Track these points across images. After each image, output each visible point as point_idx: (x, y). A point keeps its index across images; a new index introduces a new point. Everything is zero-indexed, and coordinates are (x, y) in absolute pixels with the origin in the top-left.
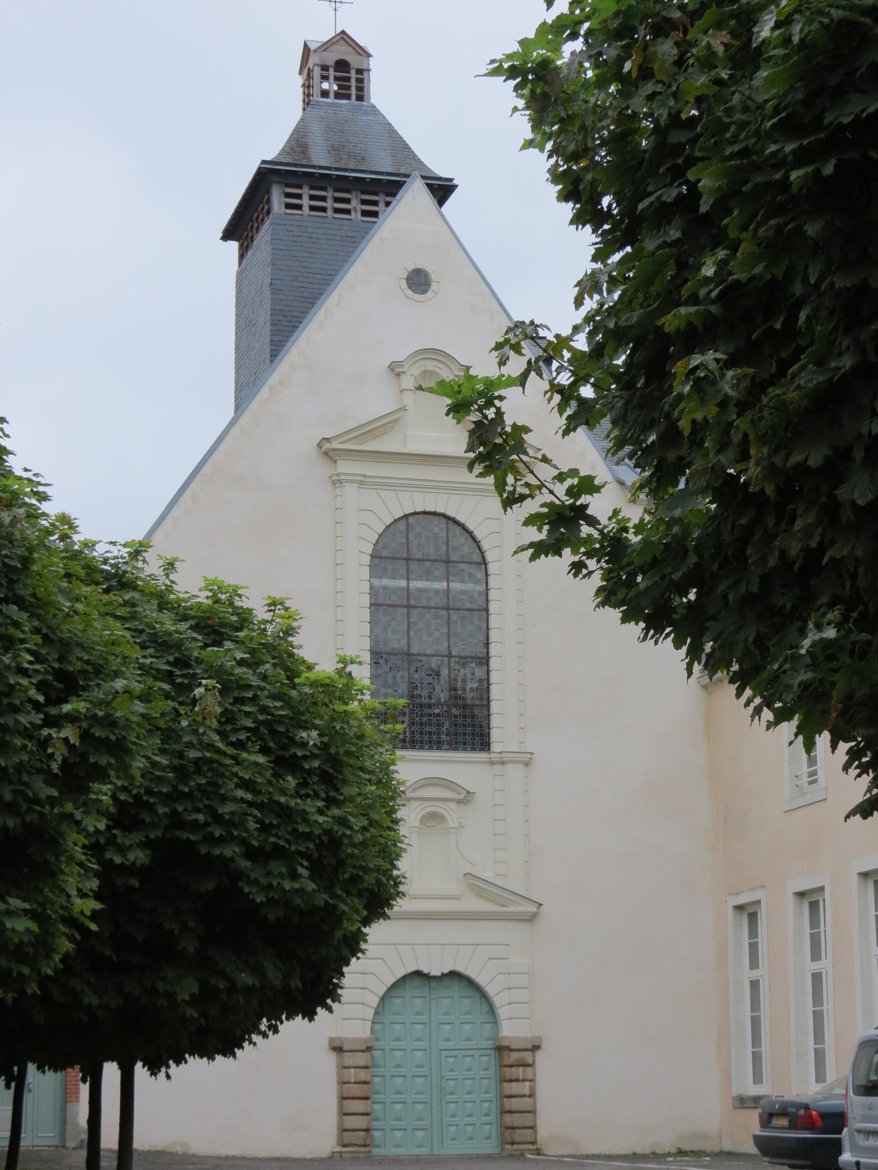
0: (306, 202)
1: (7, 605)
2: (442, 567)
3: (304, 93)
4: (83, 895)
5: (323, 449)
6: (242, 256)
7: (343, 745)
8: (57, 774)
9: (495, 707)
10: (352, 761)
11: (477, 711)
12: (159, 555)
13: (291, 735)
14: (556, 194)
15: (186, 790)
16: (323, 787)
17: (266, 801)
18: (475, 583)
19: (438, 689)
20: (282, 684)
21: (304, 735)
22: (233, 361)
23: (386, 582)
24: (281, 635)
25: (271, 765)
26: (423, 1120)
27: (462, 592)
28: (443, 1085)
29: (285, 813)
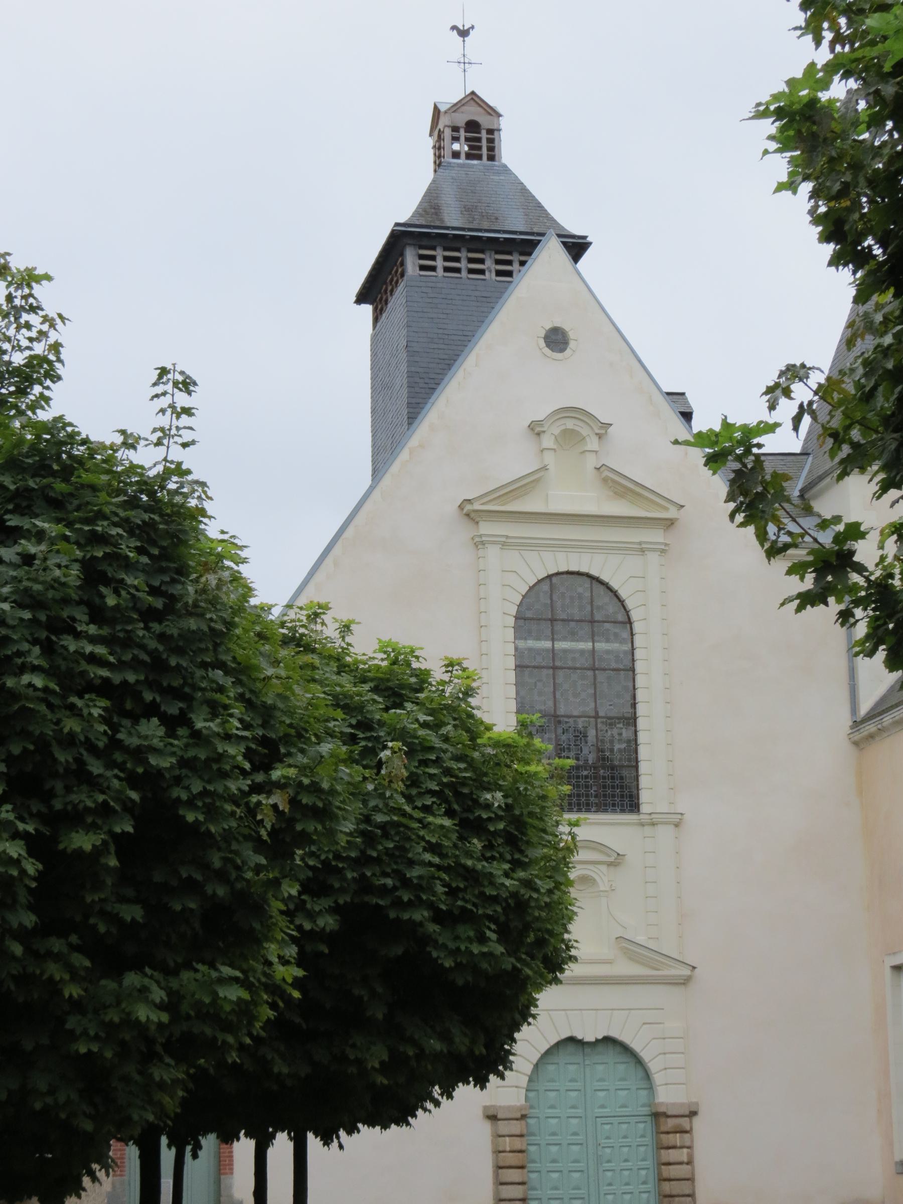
0: (440, 263)
1: (213, 670)
2: (587, 627)
3: (435, 154)
4: (284, 962)
5: (465, 511)
6: (376, 320)
7: (527, 806)
8: (266, 841)
9: (643, 767)
10: (536, 822)
11: (625, 773)
12: (334, 618)
13: (475, 797)
14: (817, 236)
15: (375, 854)
16: (508, 849)
17: (453, 864)
18: (621, 643)
19: (585, 751)
20: (464, 745)
21: (488, 796)
22: (369, 424)
23: (531, 643)
24: (461, 695)
25: (457, 828)
26: (579, 1189)
27: (608, 652)
28: (600, 1153)
29: (472, 877)
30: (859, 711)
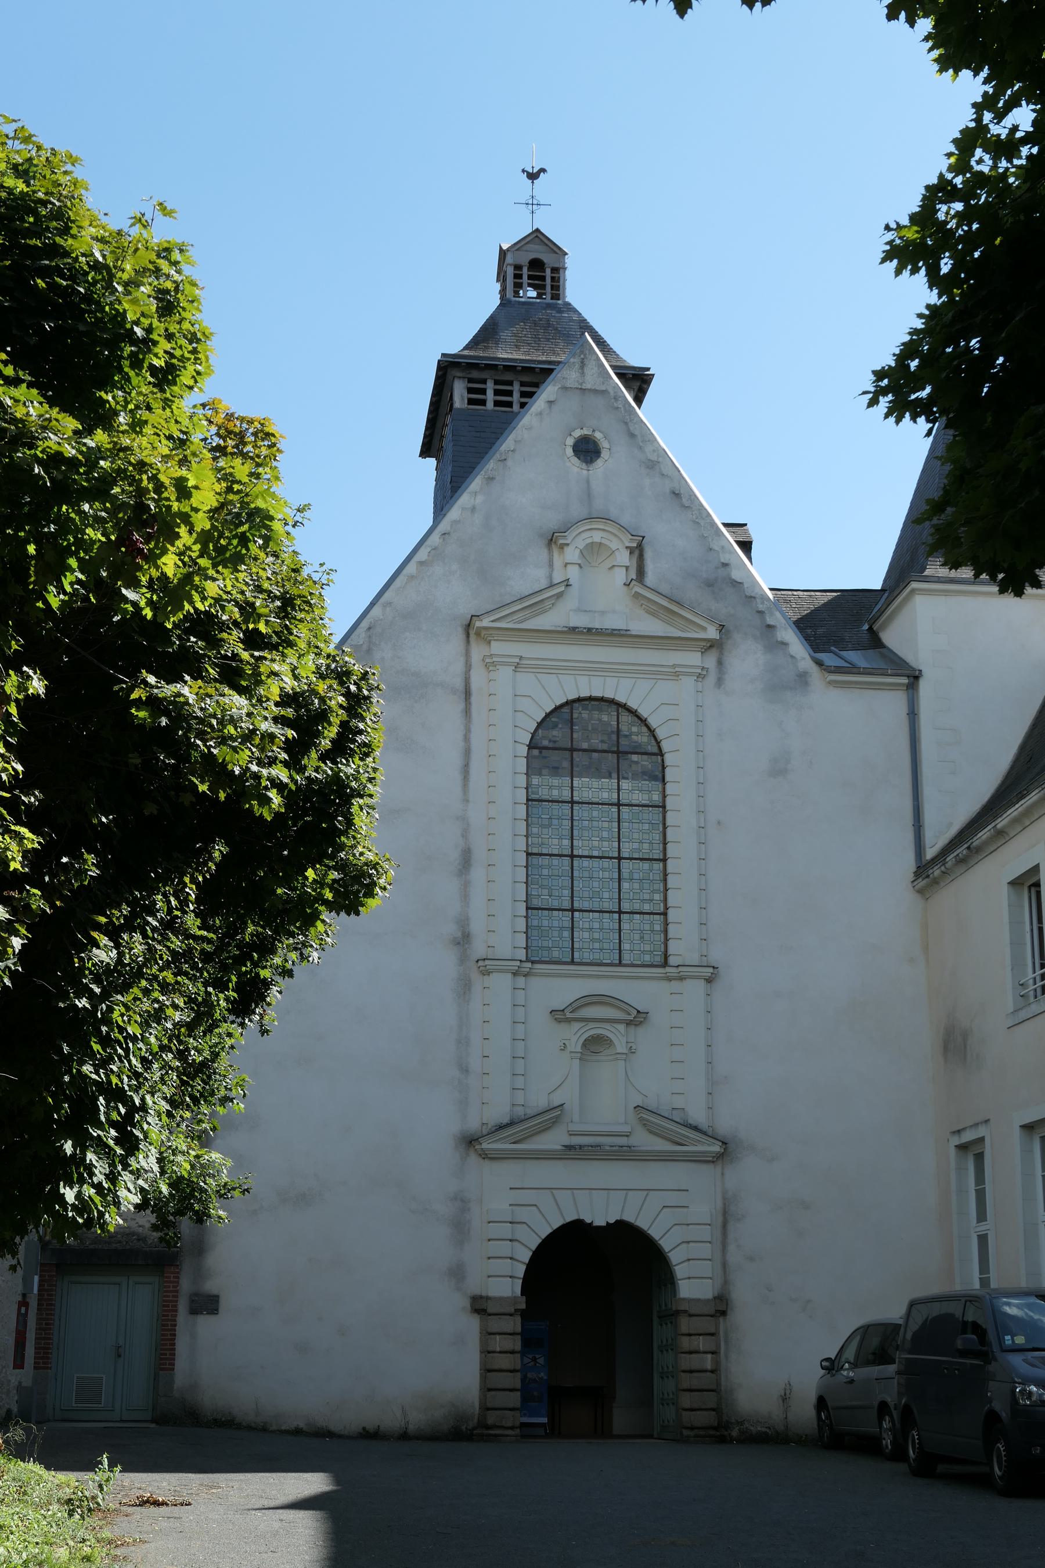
30: (925, 856)
